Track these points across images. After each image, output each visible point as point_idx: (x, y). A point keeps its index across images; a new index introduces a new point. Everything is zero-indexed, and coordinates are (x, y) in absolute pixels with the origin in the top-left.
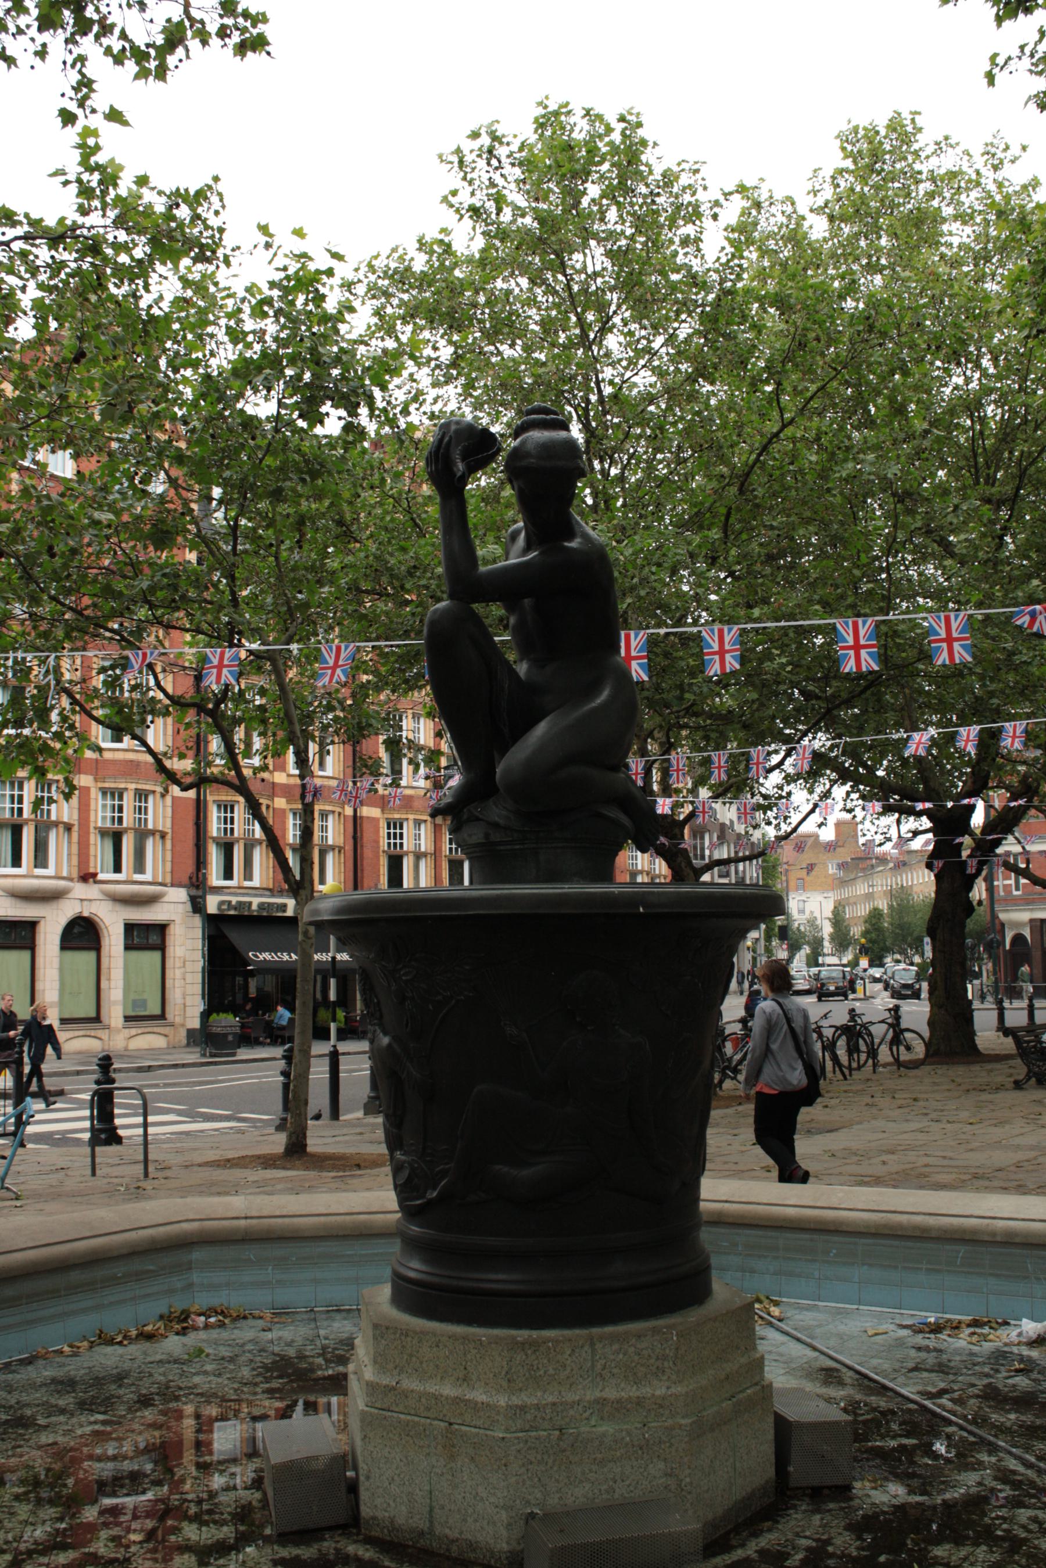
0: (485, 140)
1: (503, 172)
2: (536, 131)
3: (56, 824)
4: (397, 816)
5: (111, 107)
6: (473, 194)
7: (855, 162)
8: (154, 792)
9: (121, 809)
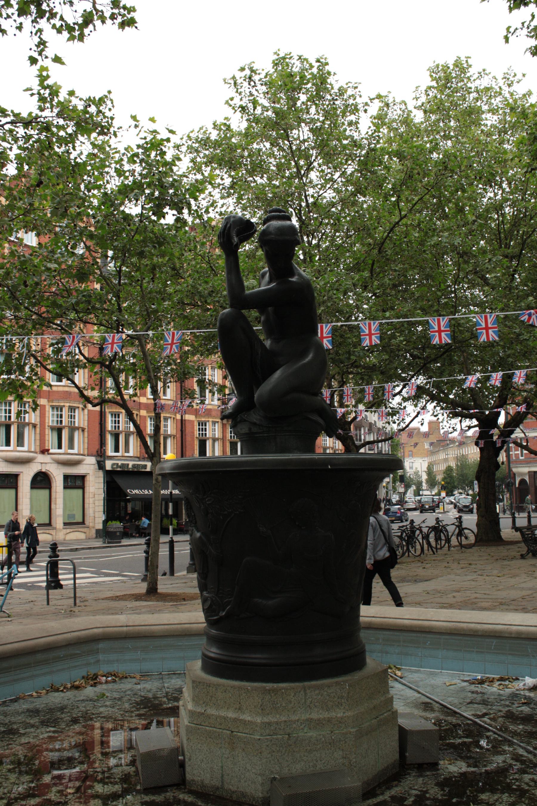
0: (247, 72)
1: (257, 88)
2: (273, 68)
3: (28, 424)
4: (203, 419)
5: (56, 55)
6: (241, 100)
7: (437, 83)
8: (78, 407)
9: (61, 416)
